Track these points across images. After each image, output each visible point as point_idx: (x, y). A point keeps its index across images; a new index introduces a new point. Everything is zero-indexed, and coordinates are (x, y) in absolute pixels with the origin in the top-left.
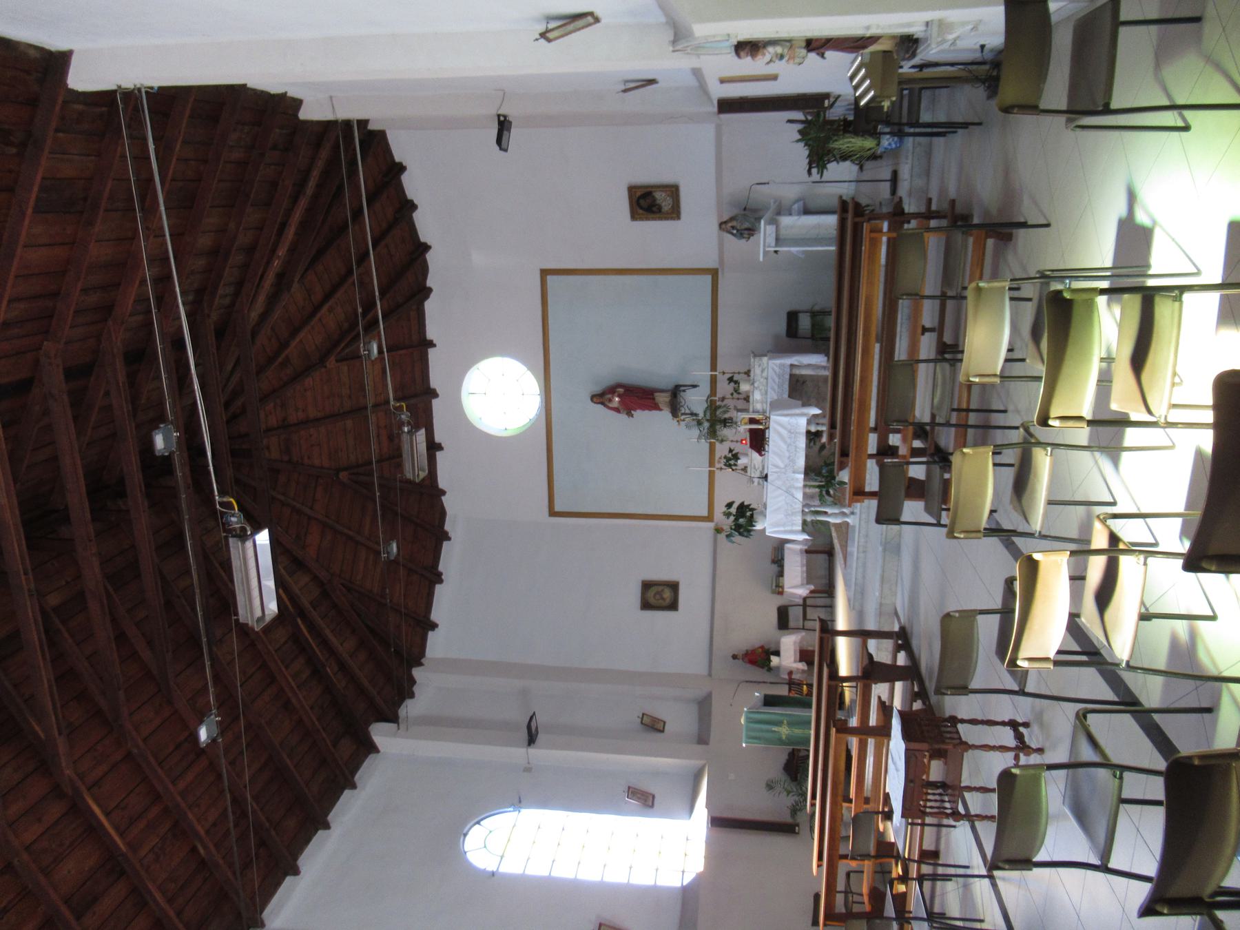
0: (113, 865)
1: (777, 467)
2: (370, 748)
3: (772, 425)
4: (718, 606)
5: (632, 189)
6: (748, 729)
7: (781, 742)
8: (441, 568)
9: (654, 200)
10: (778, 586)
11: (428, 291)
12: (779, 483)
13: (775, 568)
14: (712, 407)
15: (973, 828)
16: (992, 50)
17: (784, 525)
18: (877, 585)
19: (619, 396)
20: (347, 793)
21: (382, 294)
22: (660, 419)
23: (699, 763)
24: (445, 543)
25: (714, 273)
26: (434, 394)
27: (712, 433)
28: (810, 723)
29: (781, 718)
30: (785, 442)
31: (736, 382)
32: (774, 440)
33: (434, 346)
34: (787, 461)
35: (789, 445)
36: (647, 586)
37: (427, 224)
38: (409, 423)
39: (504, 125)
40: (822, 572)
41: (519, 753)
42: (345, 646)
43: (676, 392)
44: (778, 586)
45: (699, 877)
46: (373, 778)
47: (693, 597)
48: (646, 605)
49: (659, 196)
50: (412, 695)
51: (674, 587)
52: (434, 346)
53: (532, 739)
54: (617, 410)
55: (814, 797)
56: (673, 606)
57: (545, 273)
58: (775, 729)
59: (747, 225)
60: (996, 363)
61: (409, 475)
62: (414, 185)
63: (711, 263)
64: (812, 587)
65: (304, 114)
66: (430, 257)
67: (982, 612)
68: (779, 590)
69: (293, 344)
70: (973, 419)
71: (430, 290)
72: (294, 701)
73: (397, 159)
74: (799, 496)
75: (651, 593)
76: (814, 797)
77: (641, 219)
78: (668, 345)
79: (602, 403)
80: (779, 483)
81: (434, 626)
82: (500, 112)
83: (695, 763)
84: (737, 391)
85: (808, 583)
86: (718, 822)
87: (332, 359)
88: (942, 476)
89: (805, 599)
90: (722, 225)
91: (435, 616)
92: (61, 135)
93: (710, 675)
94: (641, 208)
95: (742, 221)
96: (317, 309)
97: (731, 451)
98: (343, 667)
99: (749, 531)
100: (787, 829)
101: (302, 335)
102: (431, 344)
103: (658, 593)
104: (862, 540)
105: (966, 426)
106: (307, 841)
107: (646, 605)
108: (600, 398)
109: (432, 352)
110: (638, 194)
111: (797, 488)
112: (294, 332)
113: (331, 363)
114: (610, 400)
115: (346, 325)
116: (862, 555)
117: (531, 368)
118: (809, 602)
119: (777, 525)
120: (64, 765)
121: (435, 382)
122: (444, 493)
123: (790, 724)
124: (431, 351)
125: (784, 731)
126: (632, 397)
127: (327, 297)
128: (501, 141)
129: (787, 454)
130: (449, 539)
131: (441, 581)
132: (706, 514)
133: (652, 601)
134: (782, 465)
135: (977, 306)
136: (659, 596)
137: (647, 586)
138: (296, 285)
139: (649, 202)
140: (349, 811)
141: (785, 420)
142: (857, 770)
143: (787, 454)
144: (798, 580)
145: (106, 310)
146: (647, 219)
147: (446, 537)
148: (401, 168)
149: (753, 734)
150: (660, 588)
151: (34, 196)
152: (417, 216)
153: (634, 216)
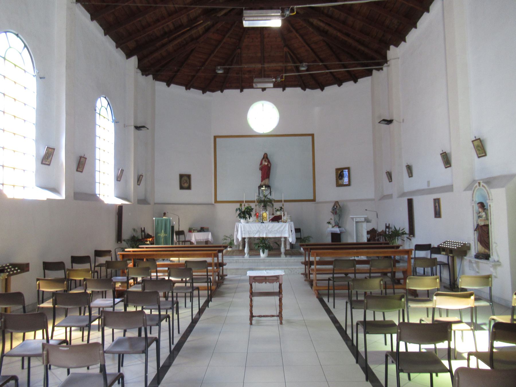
1: (268, 226)
2: (129, 55)
3: (285, 224)
4: (183, 206)
6: (162, 220)
7: (157, 233)
8: (192, 89)
10: (194, 230)
11: (304, 89)
12: (261, 227)
13: (199, 229)
14: (270, 201)
17: (244, 230)
19: (267, 165)
20: (114, 44)
21: (331, 72)
23: (132, 200)
25: (314, 200)
28: (167, 244)
29: (168, 233)
30: (278, 229)
31: (281, 210)
32: (276, 225)
33: (283, 91)
35: (277, 231)
36: (189, 176)
37: (332, 90)
38: (276, 81)
39: (137, 128)
41: (132, 123)
42: (170, 47)
44: (194, 230)
45: (102, 202)
46: (119, 55)
48: (181, 176)
50: (143, 75)
51: (189, 188)
52: (283, 91)
53: (137, 128)
54: (261, 164)
55: (146, 248)
57: (312, 135)
60: (412, 287)
62: (348, 86)
65: (392, 47)
66: (318, 91)
67: (280, 300)
68: (190, 231)
69: (298, 35)
70: (331, 292)
71: (305, 90)
73: (359, 80)
74: (257, 236)
76: (146, 248)
80: (261, 227)
82: (394, 121)
86: (120, 208)
87: (288, 50)
88: (389, 272)
90: (337, 203)
91: (172, 86)
93: (155, 204)
95: (338, 210)
96: (309, 45)
97: (252, 209)
98: (163, 45)
100: (119, 238)
101: (300, 39)
102: (242, 91)
103: (186, 181)
105: (329, 290)
107: (181, 176)
109: (238, 91)
112: (302, 36)
113: (286, 49)
114: (265, 161)
115: (299, 56)
116: (235, 261)
117: (275, 130)
119: (244, 227)
122: (222, 92)
124: (239, 90)
125: (162, 235)
128: (390, 122)
129: (273, 230)
131: (186, 89)
134: (269, 228)
135: (433, 279)
136: (185, 182)
137: (189, 176)
140: (108, 44)
141: (287, 228)
142: (132, 268)
143: (273, 230)
144: (197, 238)
146: (336, 175)
147: (204, 92)
149: (160, 222)
150: (188, 182)
152: (336, 86)
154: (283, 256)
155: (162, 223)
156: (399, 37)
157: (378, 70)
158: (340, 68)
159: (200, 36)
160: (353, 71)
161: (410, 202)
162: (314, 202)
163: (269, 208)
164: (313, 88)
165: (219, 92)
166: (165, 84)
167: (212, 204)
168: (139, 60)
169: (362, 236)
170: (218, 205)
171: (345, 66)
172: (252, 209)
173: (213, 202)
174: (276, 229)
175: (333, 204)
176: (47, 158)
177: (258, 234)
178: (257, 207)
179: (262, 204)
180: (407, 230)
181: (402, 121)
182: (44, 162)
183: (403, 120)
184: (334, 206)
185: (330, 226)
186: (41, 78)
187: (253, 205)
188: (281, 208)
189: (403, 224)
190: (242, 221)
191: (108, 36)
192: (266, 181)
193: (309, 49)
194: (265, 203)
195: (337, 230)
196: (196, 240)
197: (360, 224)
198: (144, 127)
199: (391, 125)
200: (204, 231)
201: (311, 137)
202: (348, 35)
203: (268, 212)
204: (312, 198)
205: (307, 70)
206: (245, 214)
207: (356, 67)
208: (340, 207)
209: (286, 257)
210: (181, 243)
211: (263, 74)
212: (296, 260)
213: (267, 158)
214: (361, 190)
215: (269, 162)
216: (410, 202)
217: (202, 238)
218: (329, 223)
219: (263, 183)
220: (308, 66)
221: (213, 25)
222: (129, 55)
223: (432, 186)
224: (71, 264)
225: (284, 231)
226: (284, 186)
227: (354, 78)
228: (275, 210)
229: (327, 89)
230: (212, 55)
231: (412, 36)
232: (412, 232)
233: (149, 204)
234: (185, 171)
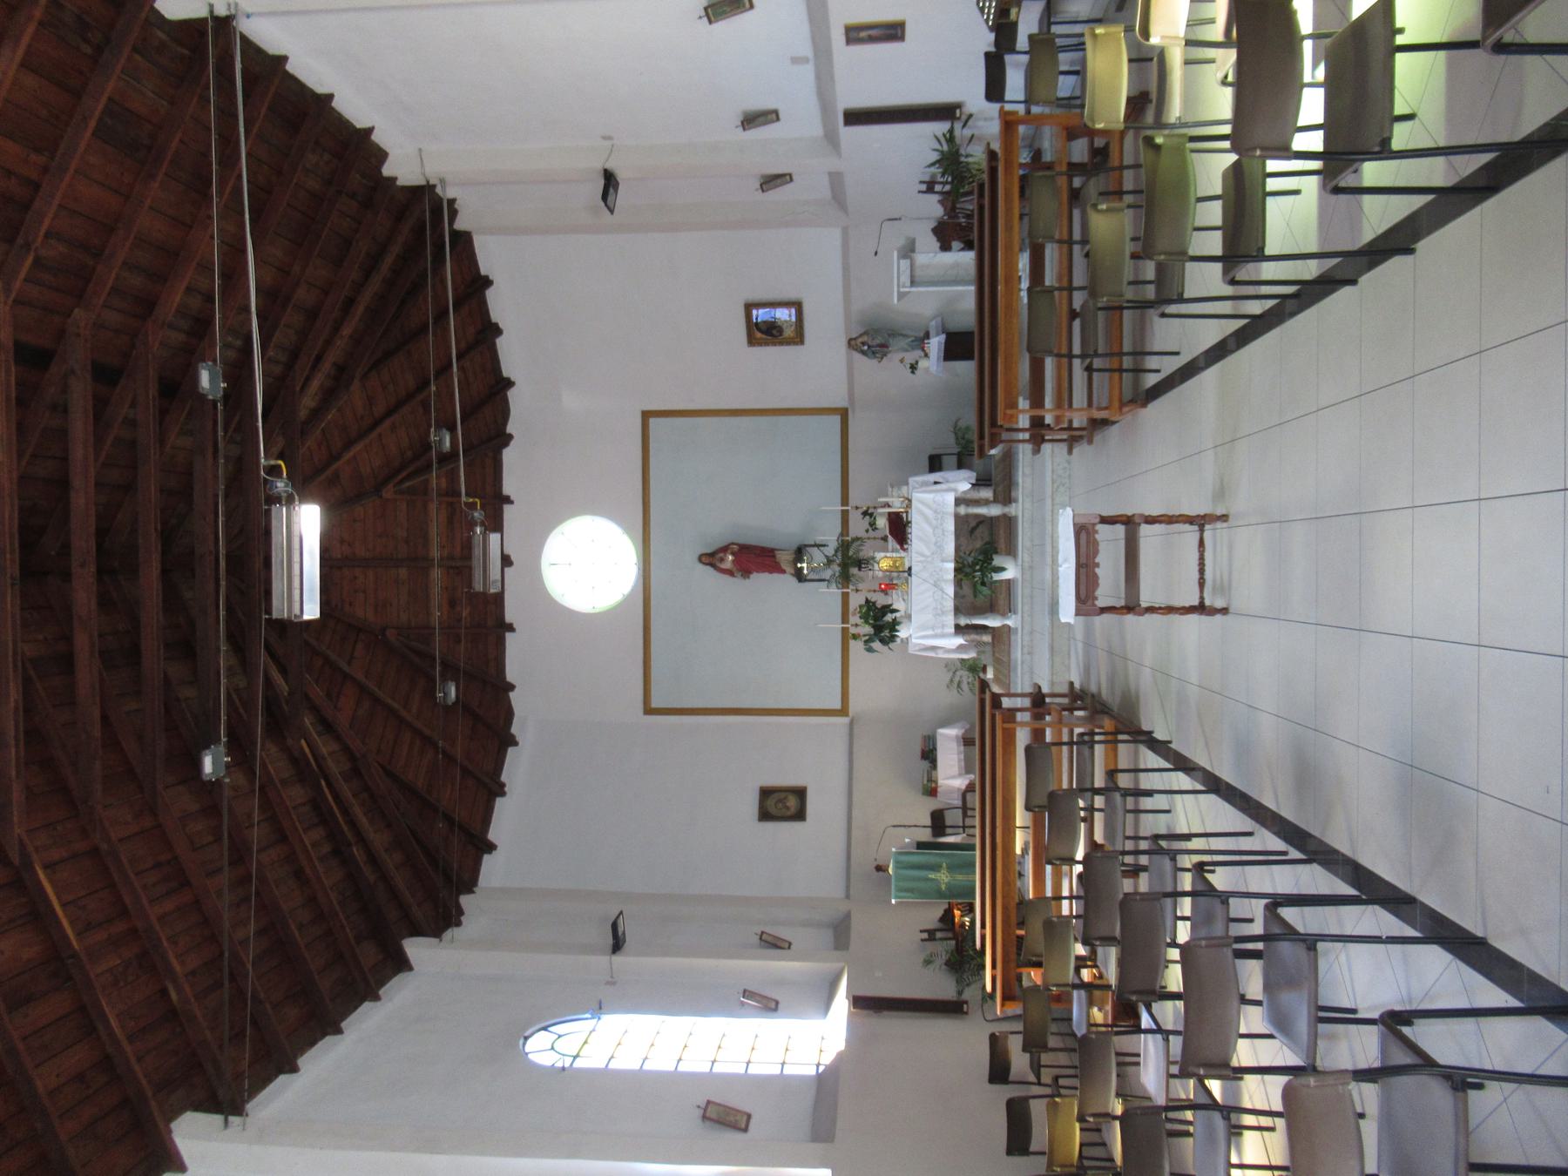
0: (58, 963)
2: (401, 964)
4: (855, 813)
6: (899, 878)
8: (504, 778)
11: (506, 439)
12: (925, 575)
13: (926, 764)
14: (844, 546)
17: (933, 628)
18: (1047, 655)
22: (783, 583)
23: (836, 966)
24: (510, 750)
25: (844, 414)
27: (845, 578)
29: (938, 860)
30: (930, 524)
35: (935, 528)
36: (766, 793)
37: (512, 355)
38: (482, 524)
39: (617, 945)
41: (602, 962)
42: (379, 839)
46: (399, 994)
48: (765, 815)
50: (459, 924)
51: (800, 793)
53: (617, 945)
54: (730, 573)
56: (800, 815)
57: (646, 415)
58: (932, 876)
59: (879, 340)
61: (478, 586)
62: (500, 304)
63: (841, 403)
66: (512, 394)
67: (1151, 520)
68: (932, 792)
69: (347, 456)
70: (1127, 362)
71: (510, 437)
72: (308, 871)
73: (483, 272)
74: (950, 590)
75: (770, 803)
77: (760, 344)
78: (793, 498)
79: (712, 565)
80: (925, 575)
81: (491, 847)
82: (608, 166)
83: (829, 966)
86: (861, 1003)
90: (851, 343)
91: (492, 836)
92: (137, 57)
93: (848, 896)
95: (873, 340)
97: (867, 601)
98: (373, 859)
100: (952, 1008)
101: (358, 447)
103: (780, 801)
104: (1027, 638)
105: (1121, 370)
106: (313, 1043)
107: (765, 815)
112: (349, 444)
113: (388, 492)
114: (722, 560)
115: (409, 454)
116: (1028, 657)
117: (628, 530)
120: (15, 819)
122: (512, 687)
123: (950, 868)
124: (507, 508)
125: (943, 877)
126: (751, 558)
127: (389, 413)
130: (515, 743)
131: (503, 794)
132: (838, 706)
133: (773, 810)
136: (783, 804)
137: (766, 793)
138: (356, 382)
141: (928, 497)
144: (955, 770)
145: (146, 305)
146: (767, 344)
148: (487, 282)
150: (782, 795)
151: (101, 107)
152: (501, 343)
154: (1011, 510)
156: (357, 149)
157: (453, 213)
158: (446, 329)
159: (346, 750)
160: (454, 290)
161: (855, 117)
163: (865, 552)
164: (504, 413)
165: (512, 695)
167: (851, 723)
168: (417, 932)
169: (956, 265)
170: (855, 706)
171: (442, 315)
172: (867, 601)
173: (845, 720)
175: (857, 356)
177: (943, 585)
178: (860, 586)
179: (854, 571)
180: (941, 127)
181: (608, 143)
183: (609, 138)
184: (863, 353)
185: (923, 364)
187: (856, 600)
188: (865, 513)
189: (922, 140)
190: (903, 633)
192: (784, 558)
193: (387, 423)
194: (849, 562)
195: (936, 344)
196: (960, 775)
197: (918, 273)
198: (615, 926)
199: (621, 175)
202: (350, 302)
203: (879, 555)
204: (837, 419)
205: (452, 429)
206: (881, 624)
207: (443, 281)
209: (1016, 501)
211: (462, 562)
212: (1027, 471)
213: (712, 555)
214: (813, 268)
215: (725, 549)
216: (855, 117)
218: (913, 368)
219: (789, 569)
220: (439, 427)
221: (314, 709)
222: (401, 964)
223: (806, 50)
224: (1032, 1157)
225: (936, 505)
226: (799, 505)
227: (476, 285)
228: (871, 534)
230: (403, 713)
231: (354, 107)
232: (946, 112)
234: (750, 804)
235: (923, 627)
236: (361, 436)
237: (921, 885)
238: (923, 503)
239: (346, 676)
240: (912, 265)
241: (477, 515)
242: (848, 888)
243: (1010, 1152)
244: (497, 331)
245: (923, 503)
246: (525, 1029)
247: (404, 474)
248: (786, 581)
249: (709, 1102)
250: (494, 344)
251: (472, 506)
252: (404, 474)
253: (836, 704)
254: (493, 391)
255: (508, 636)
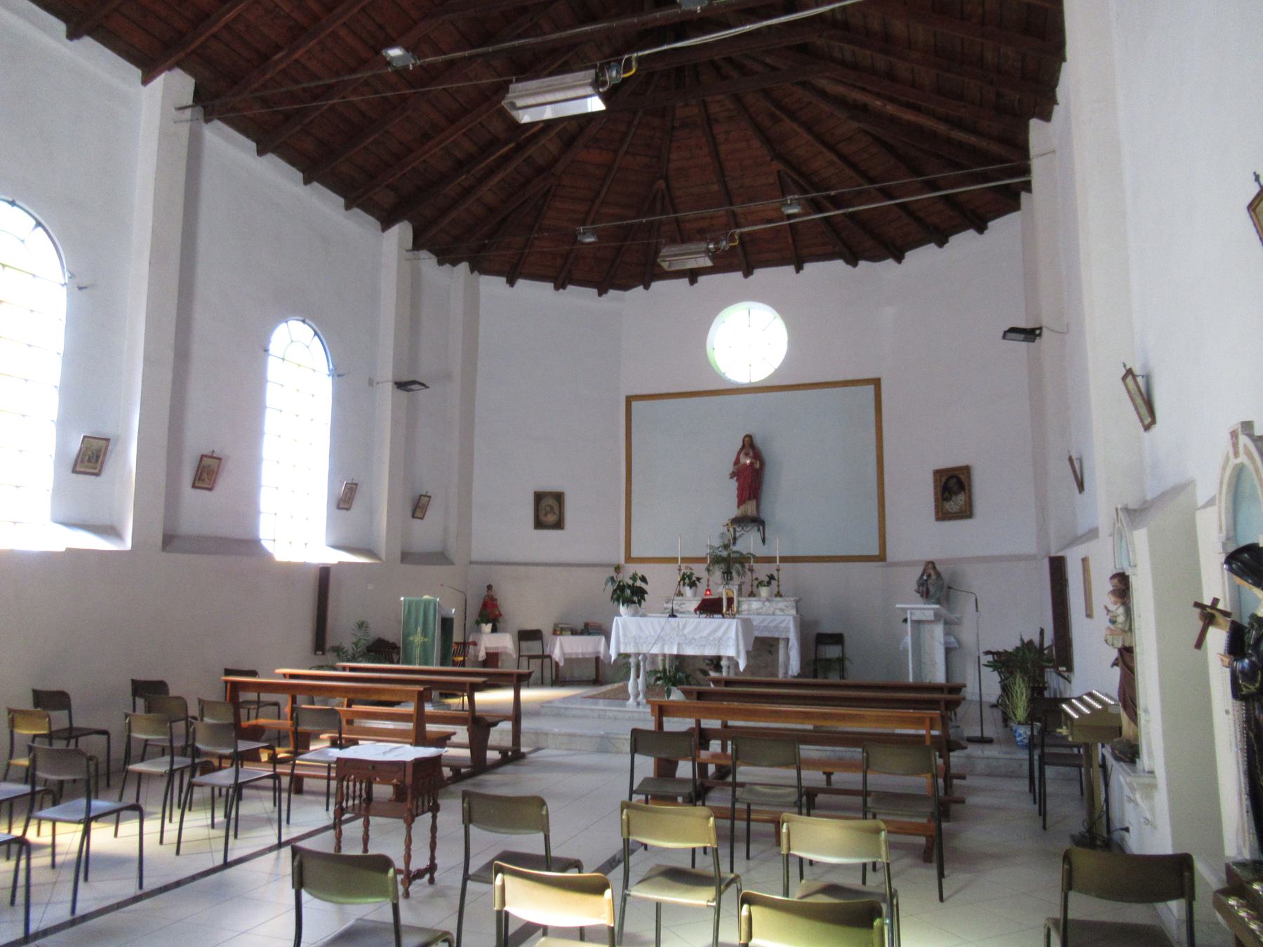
1: (684, 627)
2: (387, 222)
5: (966, 470)
6: (418, 603)
8: (570, 288)
9: (956, 494)
11: (853, 260)
13: (581, 626)
15: (326, 828)
16: (1123, 839)
17: (625, 635)
20: (341, 201)
24: (595, 291)
25: (881, 557)
26: (748, 273)
28: (426, 664)
29: (430, 634)
30: (709, 635)
31: (769, 583)
33: (798, 271)
34: (690, 637)
35: (706, 638)
36: (559, 497)
37: (923, 258)
38: (717, 249)
39: (1031, 334)
40: (577, 673)
41: (387, 373)
43: (757, 521)
46: (356, 227)
47: (548, 544)
48: (539, 497)
49: (961, 499)
50: (441, 263)
51: (559, 525)
52: (798, 271)
53: (401, 385)
54: (737, 462)
55: (352, 669)
56: (539, 524)
57: (876, 382)
58: (419, 630)
61: (664, 251)
62: (964, 242)
64: (561, 664)
66: (890, 263)
68: (558, 630)
69: (795, 126)
71: (855, 264)
73: (991, 224)
75: (551, 501)
76: (352, 669)
78: (804, 512)
79: (743, 447)
81: (511, 282)
82: (1045, 332)
83: (382, 546)
84: (761, 584)
85: (566, 660)
86: (324, 575)
89: (550, 657)
90: (931, 565)
91: (521, 283)
93: (471, 563)
94: (948, 480)
95: (936, 584)
96: (831, 148)
97: (698, 579)
98: (467, 192)
99: (618, 600)
100: (320, 642)
102: (799, 268)
105: (733, 819)
106: (292, 163)
107: (539, 497)
108: (749, 445)
110: (962, 477)
111: (663, 647)
112: (809, 128)
113: (777, 166)
114: (747, 455)
116: (596, 715)
117: (777, 372)
118: (547, 661)
121: (761, 274)
122: (647, 287)
123: (424, 644)
125: (417, 639)
126: (751, 477)
130: (600, 294)
131: (557, 288)
132: (634, 554)
133: (544, 503)
134: (686, 631)
136: (549, 510)
137: (559, 497)
138: (855, 125)
139: (953, 489)
140: (322, 204)
141: (732, 634)
144: (568, 650)
149: (413, 608)
153: (938, 473)
155: (417, 611)
156: (1055, 85)
162: (881, 563)
166: (503, 280)
173: (622, 560)
174: (705, 634)
175: (919, 570)
176: (91, 458)
182: (78, 469)
186: (80, 288)
190: (622, 609)
191: (315, 184)
193: (835, 159)
196: (564, 654)
200: (590, 634)
201: (870, 389)
202: (918, 109)
204: (876, 552)
208: (938, 575)
210: (524, 661)
214: (997, 533)
217: (580, 651)
224: (131, 699)
228: (756, 583)
229: (910, 256)
233: (451, 563)
235: (625, 627)
236: (820, 138)
237: (413, 620)
238: (727, 629)
239: (616, 152)
240: (929, 622)
241: (724, 244)
242: (481, 563)
243: (134, 682)
244: (941, 243)
245: (727, 629)
246: (312, 319)
247: (796, 177)
248: (733, 511)
249: (220, 459)
250: (929, 242)
251: (732, 239)
252: (796, 177)
253: (635, 553)
254: (894, 249)
255: (641, 288)
